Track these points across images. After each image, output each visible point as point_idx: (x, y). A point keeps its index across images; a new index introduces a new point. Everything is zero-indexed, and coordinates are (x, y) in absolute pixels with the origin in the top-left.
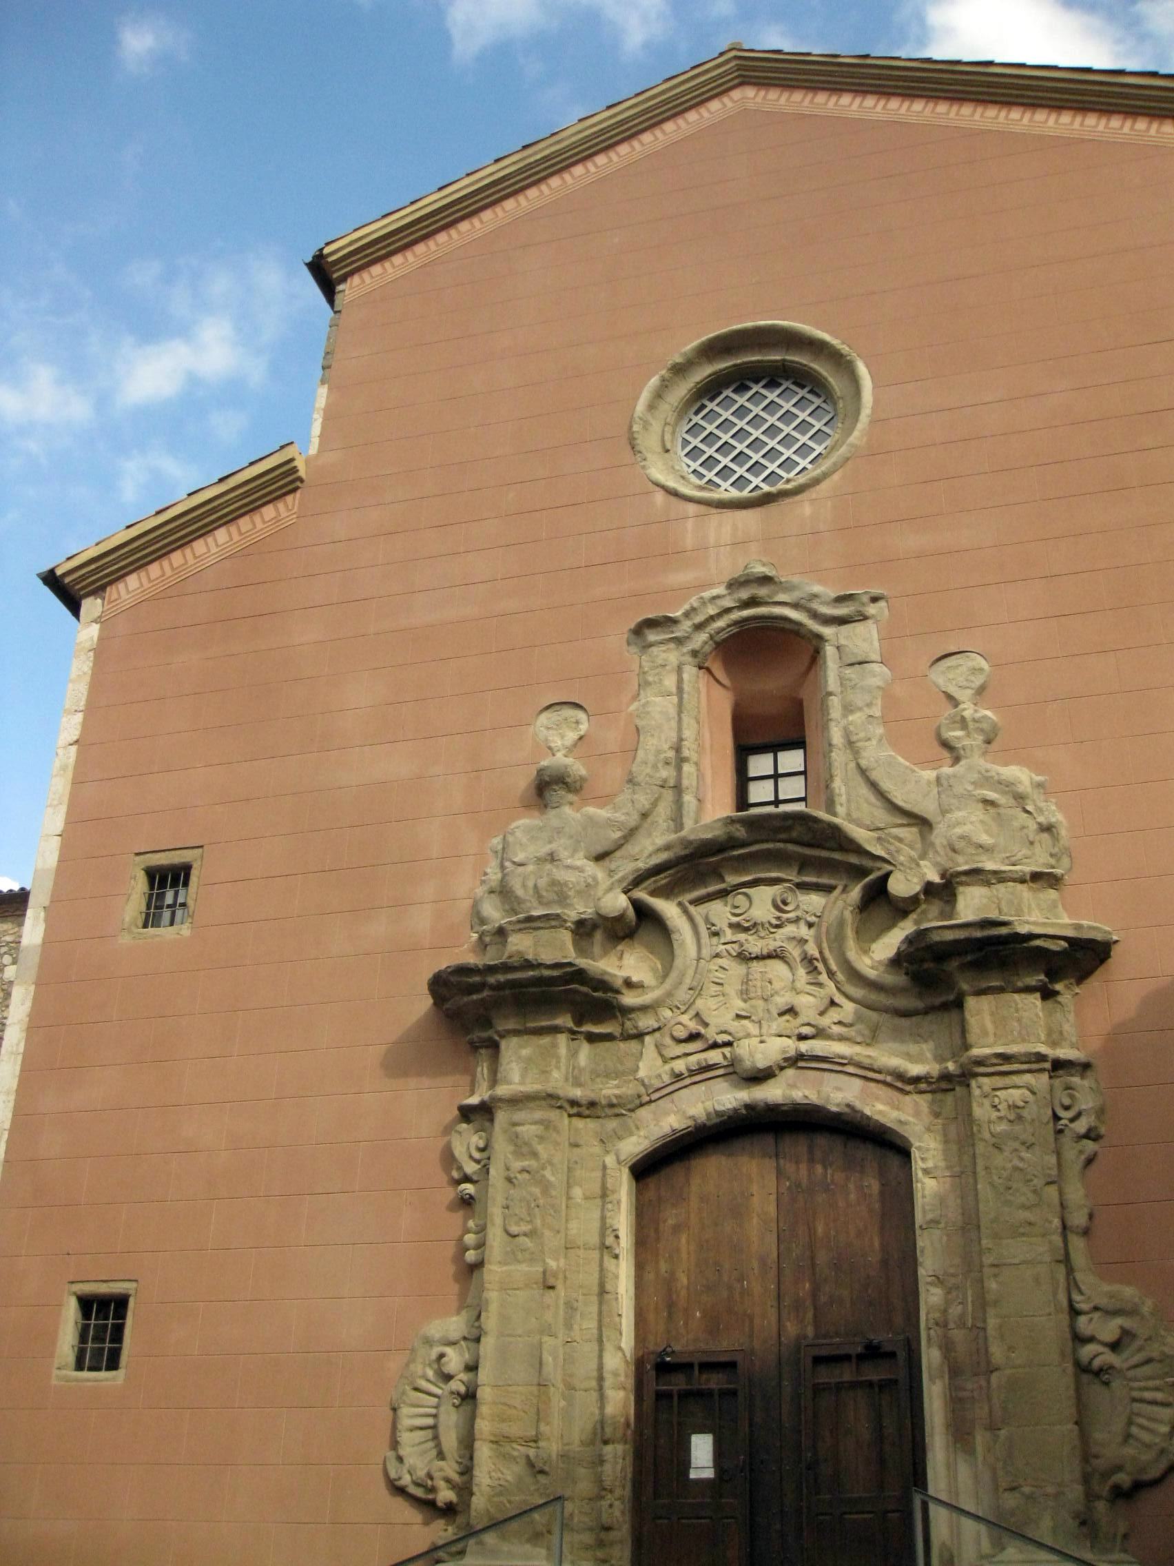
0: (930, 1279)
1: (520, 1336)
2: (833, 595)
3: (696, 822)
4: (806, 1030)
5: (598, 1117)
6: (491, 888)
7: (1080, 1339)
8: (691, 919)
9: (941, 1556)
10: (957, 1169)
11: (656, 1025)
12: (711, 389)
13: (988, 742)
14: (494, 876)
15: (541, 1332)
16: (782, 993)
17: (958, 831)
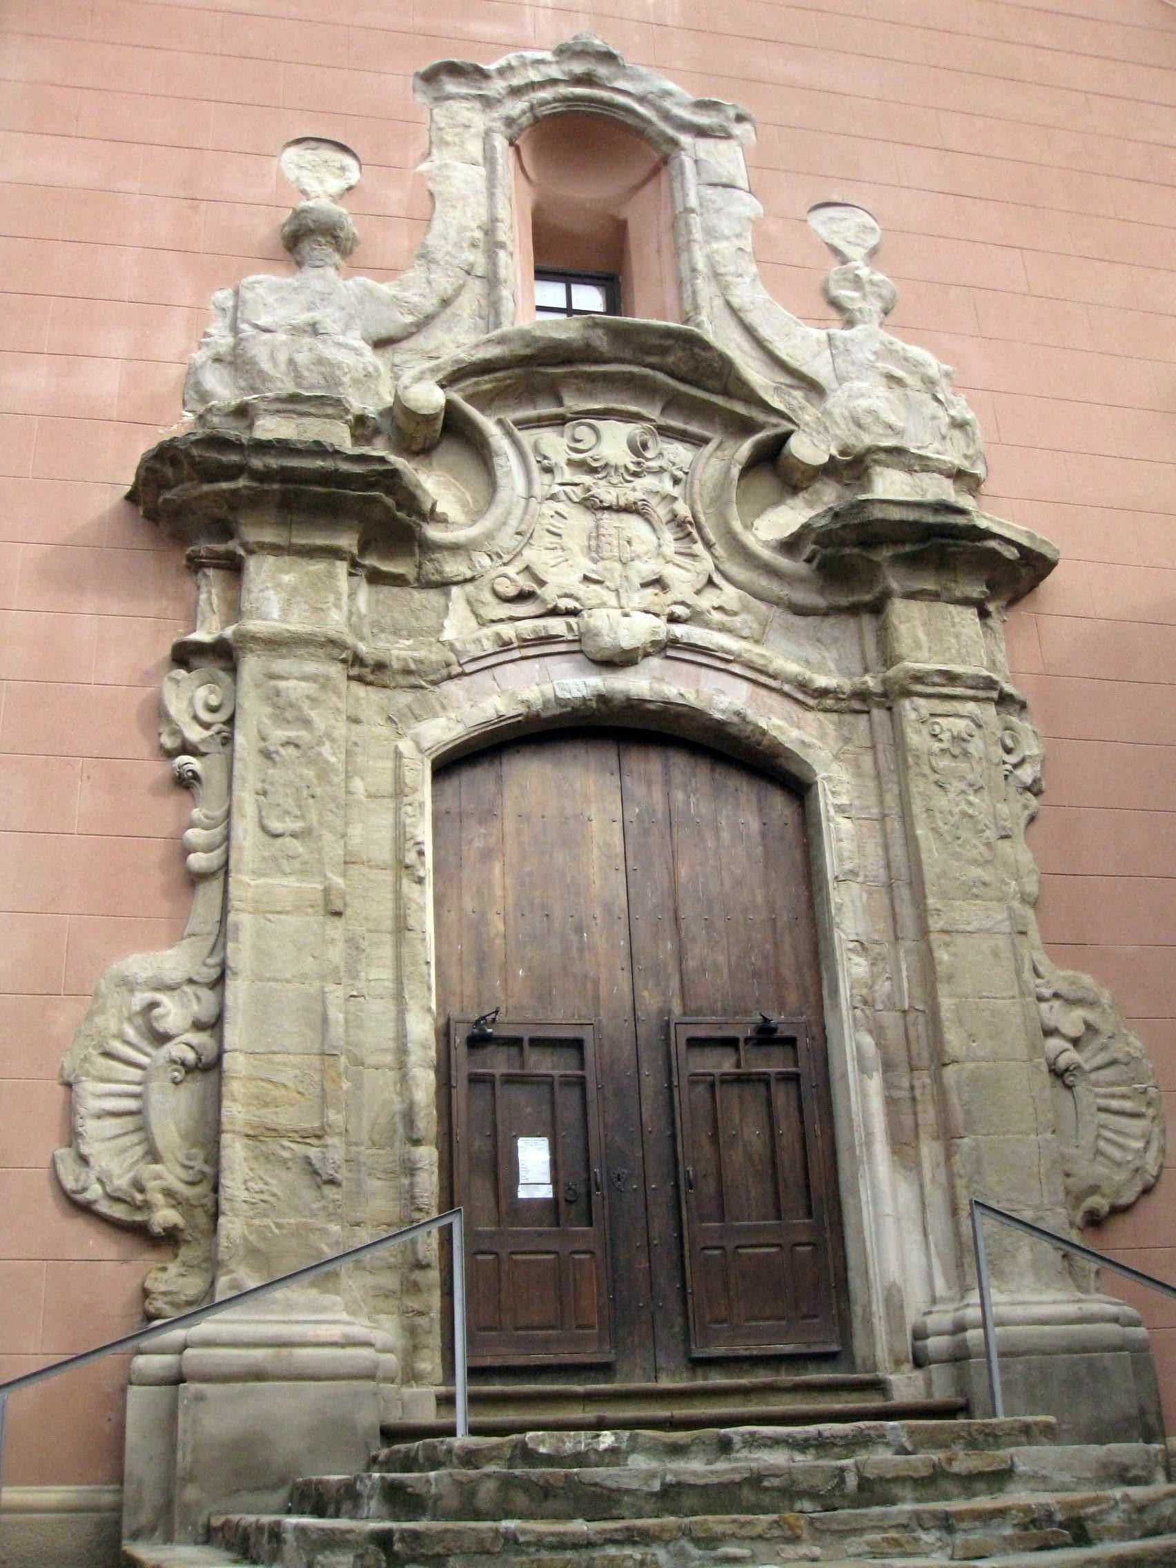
0: (851, 945)
1: (288, 981)
2: (692, 98)
4: (680, 611)
5: (385, 687)
6: (218, 353)
8: (516, 443)
11: (469, 574)
13: (886, 312)
14: (222, 339)
16: (645, 558)
17: (864, 403)
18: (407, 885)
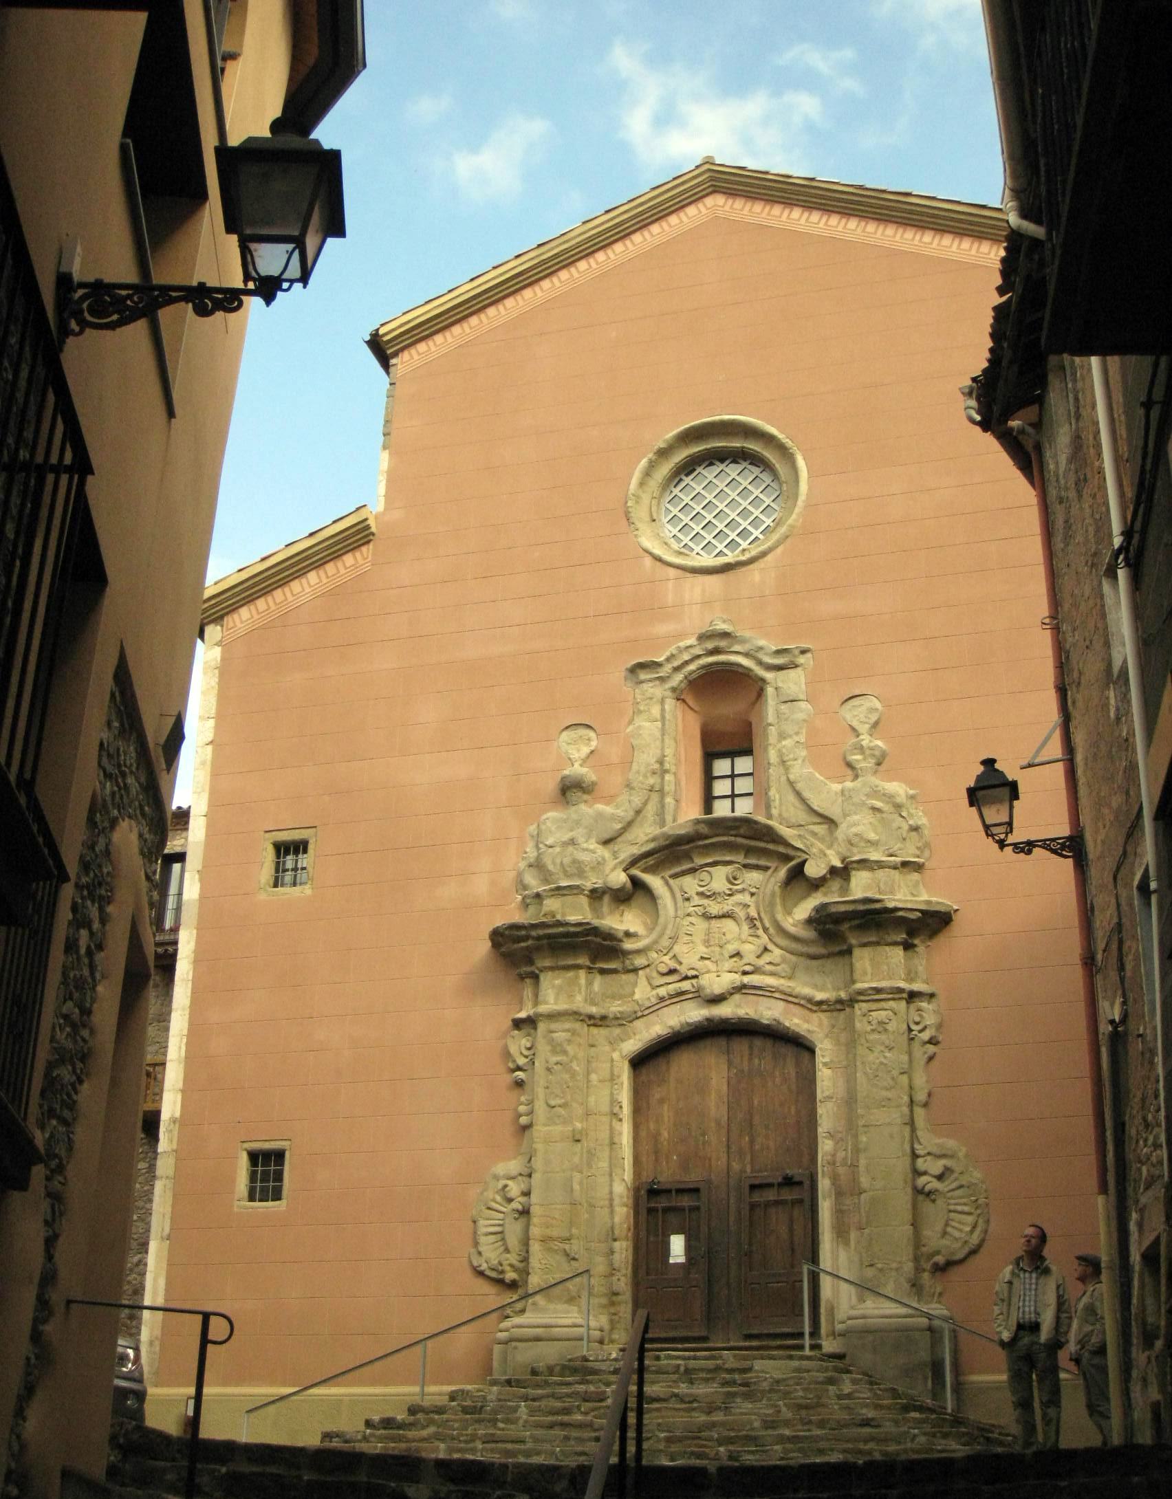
2: (774, 648)
3: (674, 820)
4: (748, 968)
7: (917, 1173)
9: (826, 1308)
10: (844, 1063)
11: (646, 963)
12: (688, 467)
13: (879, 764)
14: (532, 854)
15: (572, 1170)
17: (854, 830)
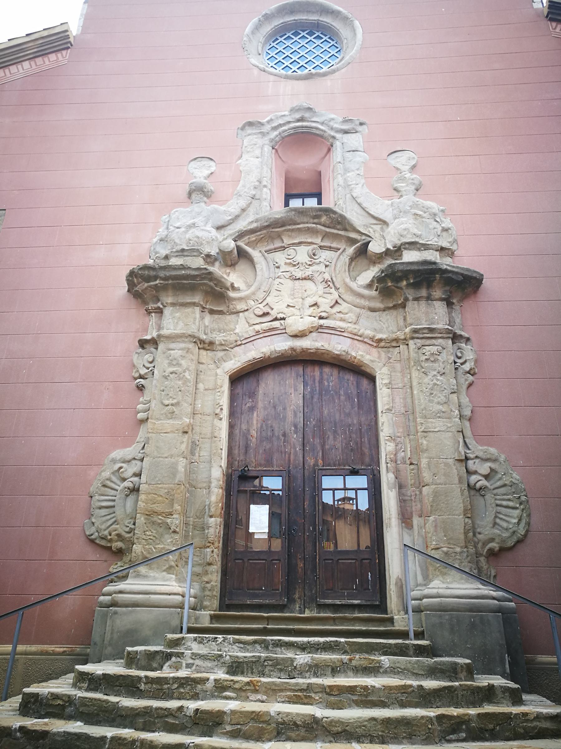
0: (387, 438)
4: (324, 314)
7: (469, 473)
11: (246, 309)
17: (403, 226)
18: (216, 421)
